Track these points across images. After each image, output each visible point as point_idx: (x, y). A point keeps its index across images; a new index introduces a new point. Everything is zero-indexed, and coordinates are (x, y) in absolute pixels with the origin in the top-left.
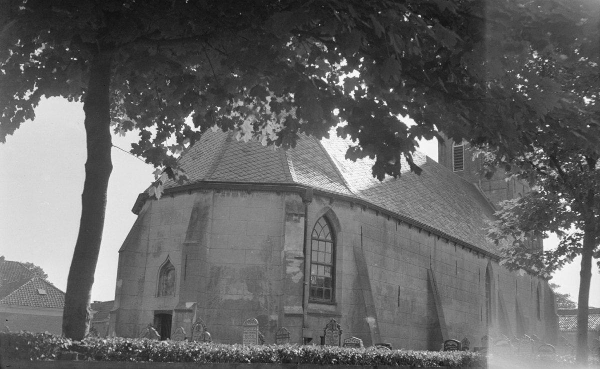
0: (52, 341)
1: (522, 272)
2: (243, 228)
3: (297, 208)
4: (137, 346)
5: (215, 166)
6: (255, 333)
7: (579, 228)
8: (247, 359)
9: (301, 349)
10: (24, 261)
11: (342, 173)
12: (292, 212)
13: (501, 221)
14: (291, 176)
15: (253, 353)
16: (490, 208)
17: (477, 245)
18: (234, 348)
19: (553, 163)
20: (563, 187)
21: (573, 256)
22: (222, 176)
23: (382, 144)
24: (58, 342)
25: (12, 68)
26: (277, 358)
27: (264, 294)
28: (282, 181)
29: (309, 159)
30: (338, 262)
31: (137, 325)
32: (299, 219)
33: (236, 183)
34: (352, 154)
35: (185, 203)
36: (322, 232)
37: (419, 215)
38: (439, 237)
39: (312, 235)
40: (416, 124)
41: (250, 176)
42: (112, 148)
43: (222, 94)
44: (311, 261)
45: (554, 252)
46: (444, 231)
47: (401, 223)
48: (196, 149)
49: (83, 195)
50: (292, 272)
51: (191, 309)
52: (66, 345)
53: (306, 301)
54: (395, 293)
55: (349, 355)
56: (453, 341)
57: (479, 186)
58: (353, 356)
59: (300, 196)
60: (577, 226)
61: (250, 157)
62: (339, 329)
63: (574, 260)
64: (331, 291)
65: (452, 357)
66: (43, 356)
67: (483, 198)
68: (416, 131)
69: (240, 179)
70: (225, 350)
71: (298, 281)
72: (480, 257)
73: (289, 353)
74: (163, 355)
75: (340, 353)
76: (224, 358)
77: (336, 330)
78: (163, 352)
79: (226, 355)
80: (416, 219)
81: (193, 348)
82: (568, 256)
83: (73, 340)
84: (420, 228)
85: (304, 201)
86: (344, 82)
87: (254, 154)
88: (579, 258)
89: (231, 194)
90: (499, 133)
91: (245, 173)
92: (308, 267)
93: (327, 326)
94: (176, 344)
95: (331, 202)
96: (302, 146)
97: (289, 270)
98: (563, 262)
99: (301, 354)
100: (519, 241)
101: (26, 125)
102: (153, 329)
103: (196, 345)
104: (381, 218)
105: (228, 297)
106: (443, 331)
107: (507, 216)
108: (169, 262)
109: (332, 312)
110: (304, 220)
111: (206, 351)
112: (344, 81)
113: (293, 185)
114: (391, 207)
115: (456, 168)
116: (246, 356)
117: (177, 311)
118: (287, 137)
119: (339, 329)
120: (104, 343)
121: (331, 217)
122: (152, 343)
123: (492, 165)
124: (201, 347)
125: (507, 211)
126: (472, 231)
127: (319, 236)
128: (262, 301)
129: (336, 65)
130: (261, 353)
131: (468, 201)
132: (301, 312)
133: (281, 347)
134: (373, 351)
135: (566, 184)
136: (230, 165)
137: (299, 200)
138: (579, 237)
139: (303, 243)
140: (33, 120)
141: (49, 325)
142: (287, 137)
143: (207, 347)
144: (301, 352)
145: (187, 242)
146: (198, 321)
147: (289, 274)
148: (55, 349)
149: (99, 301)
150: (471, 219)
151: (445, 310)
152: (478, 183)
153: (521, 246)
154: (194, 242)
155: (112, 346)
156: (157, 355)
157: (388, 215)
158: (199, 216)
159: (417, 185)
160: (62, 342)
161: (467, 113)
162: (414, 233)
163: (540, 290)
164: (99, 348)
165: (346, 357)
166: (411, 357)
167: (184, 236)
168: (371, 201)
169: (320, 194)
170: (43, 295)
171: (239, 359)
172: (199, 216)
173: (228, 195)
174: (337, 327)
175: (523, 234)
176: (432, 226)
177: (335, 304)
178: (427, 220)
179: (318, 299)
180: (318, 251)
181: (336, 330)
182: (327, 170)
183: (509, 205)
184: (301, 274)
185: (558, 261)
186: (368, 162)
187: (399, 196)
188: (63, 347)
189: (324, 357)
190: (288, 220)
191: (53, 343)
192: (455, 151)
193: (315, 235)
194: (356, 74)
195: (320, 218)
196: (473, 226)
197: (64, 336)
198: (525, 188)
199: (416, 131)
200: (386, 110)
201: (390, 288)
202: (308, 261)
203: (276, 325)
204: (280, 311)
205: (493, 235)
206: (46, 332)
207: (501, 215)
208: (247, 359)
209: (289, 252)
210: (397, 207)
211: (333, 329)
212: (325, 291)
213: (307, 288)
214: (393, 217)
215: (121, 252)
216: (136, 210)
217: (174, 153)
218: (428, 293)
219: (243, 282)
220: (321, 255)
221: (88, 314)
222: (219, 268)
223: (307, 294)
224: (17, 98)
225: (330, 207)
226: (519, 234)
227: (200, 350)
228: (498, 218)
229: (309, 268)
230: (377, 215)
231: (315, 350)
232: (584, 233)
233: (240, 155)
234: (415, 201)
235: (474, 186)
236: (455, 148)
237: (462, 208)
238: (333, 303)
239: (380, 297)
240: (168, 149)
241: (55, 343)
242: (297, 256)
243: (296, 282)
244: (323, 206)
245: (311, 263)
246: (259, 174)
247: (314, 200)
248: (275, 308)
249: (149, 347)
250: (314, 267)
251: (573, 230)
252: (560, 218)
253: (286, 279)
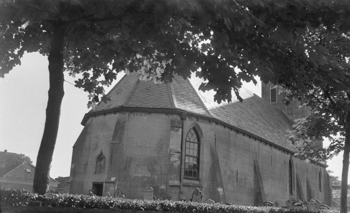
0: (26, 195)
1: (307, 161)
2: (145, 133)
3: (177, 123)
4: (77, 199)
5: (129, 99)
6: (151, 196)
7: (342, 135)
8: (142, 208)
9: (174, 203)
10: (19, 153)
11: (204, 102)
12: (175, 125)
13: (296, 131)
14: (174, 104)
15: (146, 205)
16: (291, 123)
17: (284, 147)
18: (134, 202)
19: (326, 95)
20: (332, 110)
21: (339, 151)
22: (134, 104)
23: (222, 83)
24: (30, 195)
25: (9, 36)
26: (160, 208)
27: (157, 173)
28: (169, 107)
29: (185, 94)
30: (201, 155)
31: (83, 191)
32: (179, 129)
33: (142, 108)
34: (203, 88)
35: (112, 119)
36: (192, 138)
37: (250, 128)
38: (261, 141)
39: (186, 139)
40: (241, 72)
41: (150, 104)
42: (64, 82)
43: (130, 52)
44: (185, 154)
45: (327, 149)
46: (264, 138)
47: (239, 133)
48: (118, 88)
49: (47, 110)
50: (174, 160)
51: (114, 181)
52: (34, 197)
53: (182, 177)
54: (235, 174)
55: (203, 207)
56: (270, 203)
57: (285, 112)
58: (206, 208)
59: (180, 116)
60: (341, 134)
61: (150, 93)
63: (339, 154)
64: (197, 173)
65: (265, 209)
66: (20, 203)
67: (288, 119)
68: (242, 76)
69: (144, 106)
70: (129, 203)
71: (177, 166)
72: (286, 154)
73: (167, 205)
74: (92, 204)
75: (198, 206)
76: (128, 207)
77: (199, 195)
78: (92, 202)
79: (129, 205)
80: (248, 130)
81: (110, 201)
82: (335, 151)
83: (39, 195)
84: (250, 136)
85: (181, 119)
86: (201, 46)
87: (152, 91)
88: (342, 153)
89: (139, 114)
90: (291, 78)
91: (147, 102)
92: (183, 158)
93: (194, 193)
94: (100, 198)
95: (197, 120)
96: (181, 86)
97: (172, 159)
98: (333, 155)
99: (174, 205)
100: (307, 142)
101: (16, 68)
102: (91, 192)
103: (112, 199)
104: (227, 129)
105: (136, 175)
106: (263, 197)
107: (300, 128)
108: (102, 153)
109: (197, 184)
110: (181, 130)
111: (117, 203)
112: (201, 45)
113: (174, 109)
114: (233, 123)
115: (272, 101)
116: (142, 206)
117: (106, 182)
118: (167, 76)
120: (57, 196)
121: (197, 129)
122: (86, 197)
123: (290, 97)
124: (114, 200)
125: (300, 124)
126: (281, 138)
127: (190, 140)
128: (156, 177)
129: (196, 35)
130: (150, 205)
131: (279, 121)
132: (179, 184)
133: (162, 202)
134: (218, 205)
135: (335, 108)
136: (139, 97)
137: (179, 118)
138: (342, 140)
139: (180, 144)
140: (20, 65)
141: (26, 186)
142: (167, 76)
143: (118, 200)
144: (174, 205)
145: (112, 142)
146: (118, 189)
147: (172, 162)
148: (28, 199)
149: (62, 176)
150: (280, 131)
151: (264, 185)
152: (285, 110)
153: (309, 145)
154: (116, 142)
155: (62, 198)
156: (88, 204)
157: (231, 128)
158: (120, 127)
159: (249, 110)
160: (32, 195)
161: (272, 66)
162: (246, 138)
163: (321, 174)
164: (54, 199)
165: (201, 208)
166: (240, 209)
167: (111, 139)
168: (221, 119)
169: (191, 115)
170: (29, 172)
171: (138, 208)
172: (120, 127)
173: (137, 115)
175: (309, 138)
176: (257, 135)
177: (199, 180)
178: (254, 131)
179: (189, 177)
180: (190, 149)
181: (199, 195)
182: (195, 101)
183: (300, 121)
184: (179, 162)
185: (330, 154)
186: (212, 93)
187: (238, 117)
188: (32, 198)
189: (188, 208)
190: (172, 130)
191: (27, 195)
192: (271, 91)
193: (188, 139)
194: (208, 41)
195: (191, 129)
196: (281, 135)
197: (33, 192)
199: (242, 76)
200: (225, 62)
201: (232, 171)
202: (183, 155)
203: (164, 192)
204: (167, 183)
205: (292, 139)
206: (24, 190)
207: (296, 127)
208: (142, 208)
209: (172, 149)
210: (237, 124)
211: (197, 195)
212: (193, 172)
213: (183, 171)
214: (234, 129)
215: (74, 147)
216: (83, 123)
217: (103, 85)
218: (255, 174)
219: (144, 166)
220: (191, 151)
221: (48, 179)
222: (131, 158)
223: (183, 174)
224: (10, 52)
225: (197, 122)
226: (307, 138)
227: (114, 202)
228: (294, 129)
229: (184, 158)
230: (225, 128)
231: (183, 204)
232: (345, 138)
233: (144, 92)
234: (247, 120)
235: (282, 112)
236: (271, 89)
237: (275, 125)
238: (198, 179)
239: (225, 176)
240: (100, 83)
241: (28, 196)
242: (177, 151)
243: (176, 166)
244: (193, 122)
245: (185, 155)
246: (155, 103)
247: (187, 119)
248: (163, 182)
249: (84, 199)
250: (187, 158)
251: (338, 136)
252: (331, 129)
253: (171, 165)
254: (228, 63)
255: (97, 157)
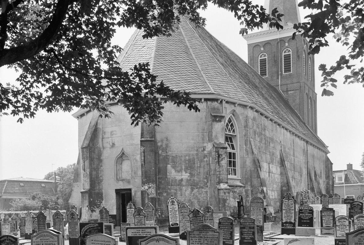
6: (191, 221)
62: (294, 199)
119: (294, 199)
174: (292, 198)
198: (310, 89)
211: (289, 199)
254: (2, 43)
255: (117, 158)
